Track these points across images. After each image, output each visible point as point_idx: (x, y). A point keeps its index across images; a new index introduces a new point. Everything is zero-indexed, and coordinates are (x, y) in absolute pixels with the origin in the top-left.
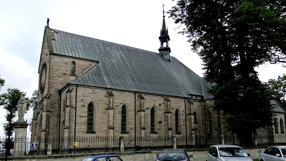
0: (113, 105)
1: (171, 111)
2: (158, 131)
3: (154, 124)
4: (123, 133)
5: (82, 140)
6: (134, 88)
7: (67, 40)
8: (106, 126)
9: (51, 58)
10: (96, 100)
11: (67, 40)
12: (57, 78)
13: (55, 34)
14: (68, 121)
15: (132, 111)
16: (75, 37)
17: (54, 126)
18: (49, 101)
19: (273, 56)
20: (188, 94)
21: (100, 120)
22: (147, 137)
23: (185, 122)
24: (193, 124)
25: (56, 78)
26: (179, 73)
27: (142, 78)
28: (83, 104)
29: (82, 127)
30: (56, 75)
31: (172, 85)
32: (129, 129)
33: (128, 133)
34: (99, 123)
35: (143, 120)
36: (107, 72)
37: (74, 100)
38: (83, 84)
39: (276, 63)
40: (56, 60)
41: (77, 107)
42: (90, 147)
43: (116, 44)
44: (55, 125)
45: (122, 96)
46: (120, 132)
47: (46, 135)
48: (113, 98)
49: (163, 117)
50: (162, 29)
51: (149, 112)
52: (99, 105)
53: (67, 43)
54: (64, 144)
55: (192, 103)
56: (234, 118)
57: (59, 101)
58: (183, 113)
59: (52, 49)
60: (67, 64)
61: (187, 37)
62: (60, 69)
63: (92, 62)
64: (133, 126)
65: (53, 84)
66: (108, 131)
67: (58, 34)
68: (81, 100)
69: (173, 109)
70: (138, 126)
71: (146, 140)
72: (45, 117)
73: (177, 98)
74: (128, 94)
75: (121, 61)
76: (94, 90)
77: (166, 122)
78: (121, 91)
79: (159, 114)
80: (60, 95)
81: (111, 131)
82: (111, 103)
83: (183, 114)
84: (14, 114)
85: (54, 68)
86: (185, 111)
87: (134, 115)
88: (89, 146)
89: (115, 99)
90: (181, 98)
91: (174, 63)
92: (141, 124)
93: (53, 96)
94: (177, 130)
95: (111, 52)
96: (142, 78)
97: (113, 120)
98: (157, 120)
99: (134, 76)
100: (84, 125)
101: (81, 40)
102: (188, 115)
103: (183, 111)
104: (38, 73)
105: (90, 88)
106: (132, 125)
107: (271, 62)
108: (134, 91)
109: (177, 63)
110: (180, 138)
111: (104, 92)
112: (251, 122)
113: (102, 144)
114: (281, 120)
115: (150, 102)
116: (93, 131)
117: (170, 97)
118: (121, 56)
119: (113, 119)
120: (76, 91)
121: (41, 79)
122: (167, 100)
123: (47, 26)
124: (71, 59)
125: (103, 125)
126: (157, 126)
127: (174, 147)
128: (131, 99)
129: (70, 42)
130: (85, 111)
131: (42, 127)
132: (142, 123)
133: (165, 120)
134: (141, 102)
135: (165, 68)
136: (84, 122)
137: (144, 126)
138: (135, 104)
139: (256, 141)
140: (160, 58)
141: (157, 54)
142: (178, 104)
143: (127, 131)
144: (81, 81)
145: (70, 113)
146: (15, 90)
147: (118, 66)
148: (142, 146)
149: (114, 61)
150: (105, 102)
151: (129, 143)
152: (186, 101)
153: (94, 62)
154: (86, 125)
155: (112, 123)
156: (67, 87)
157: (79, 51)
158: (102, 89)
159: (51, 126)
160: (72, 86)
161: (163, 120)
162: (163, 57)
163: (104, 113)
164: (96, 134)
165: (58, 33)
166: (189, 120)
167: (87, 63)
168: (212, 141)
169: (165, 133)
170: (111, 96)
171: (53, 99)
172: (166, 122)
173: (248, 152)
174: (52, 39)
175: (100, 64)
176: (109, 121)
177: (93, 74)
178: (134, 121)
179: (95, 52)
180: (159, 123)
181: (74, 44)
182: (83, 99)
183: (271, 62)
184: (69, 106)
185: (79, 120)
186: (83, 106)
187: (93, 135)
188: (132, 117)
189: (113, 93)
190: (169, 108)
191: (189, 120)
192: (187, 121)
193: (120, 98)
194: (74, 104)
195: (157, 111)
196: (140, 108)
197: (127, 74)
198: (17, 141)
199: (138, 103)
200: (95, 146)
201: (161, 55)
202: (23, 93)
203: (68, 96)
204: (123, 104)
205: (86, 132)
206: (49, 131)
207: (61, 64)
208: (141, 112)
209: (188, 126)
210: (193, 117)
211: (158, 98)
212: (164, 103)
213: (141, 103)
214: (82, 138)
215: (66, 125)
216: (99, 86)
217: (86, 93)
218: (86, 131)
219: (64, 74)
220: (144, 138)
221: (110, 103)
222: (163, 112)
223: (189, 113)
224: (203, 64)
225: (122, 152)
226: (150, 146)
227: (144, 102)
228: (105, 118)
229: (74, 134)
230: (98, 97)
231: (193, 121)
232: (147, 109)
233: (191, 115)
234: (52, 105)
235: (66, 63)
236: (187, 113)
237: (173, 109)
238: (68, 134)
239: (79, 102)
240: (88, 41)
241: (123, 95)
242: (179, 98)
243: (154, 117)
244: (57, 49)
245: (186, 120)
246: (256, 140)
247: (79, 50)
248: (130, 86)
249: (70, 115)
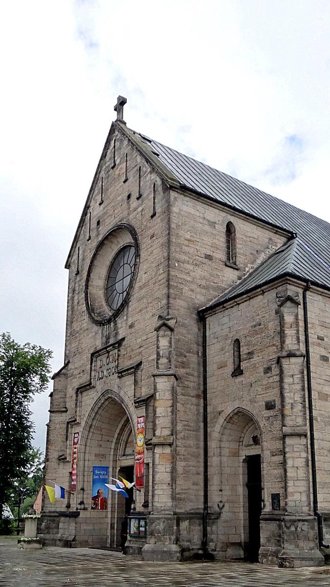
30: (187, 258)
40: (185, 208)
57: (198, 345)
85: (181, 233)
121: (90, 283)
171: (182, 335)
203: (289, 319)
215: (288, 421)
235: (212, 224)
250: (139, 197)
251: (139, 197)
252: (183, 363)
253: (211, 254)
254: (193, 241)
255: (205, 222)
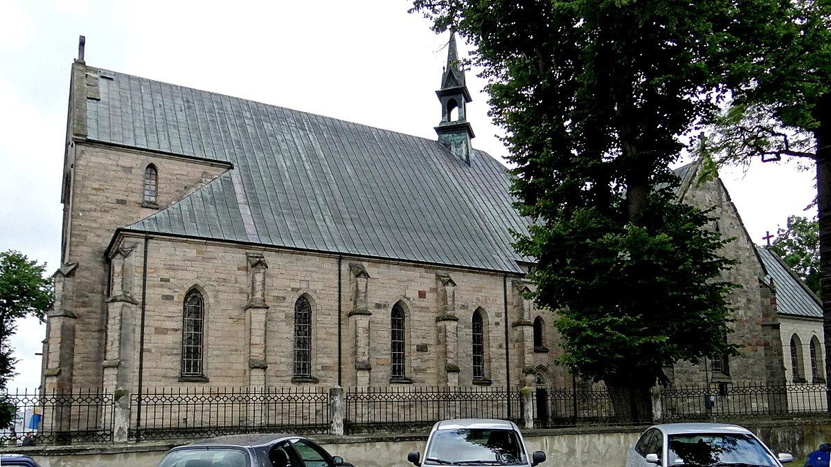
0: (263, 295)
1: (459, 313)
2: (414, 376)
3: (404, 354)
4: (300, 382)
5: (166, 400)
6: (338, 242)
7: (136, 100)
8: (242, 359)
9: (78, 153)
10: (210, 279)
11: (136, 100)
12: (99, 214)
13: (103, 82)
14: (117, 344)
15: (329, 315)
16: (166, 91)
17: (89, 359)
18: (71, 283)
19: (772, 139)
20: (517, 261)
21: (222, 343)
22: (600, 392)
23: (504, 346)
24: (530, 353)
25: (94, 214)
26: (496, 197)
27: (370, 213)
28: (167, 292)
29: (163, 365)
30: (93, 207)
31: (467, 235)
32: (319, 367)
33: (316, 381)
34: (219, 349)
35: (362, 341)
36: (255, 197)
37: (138, 281)
38: (168, 232)
39: (779, 158)
40: (94, 159)
41: (146, 300)
42: (190, 423)
43: (299, 112)
44: (92, 356)
45: (295, 268)
46: (290, 378)
47: (60, 386)
48: (264, 273)
49: (433, 333)
50: (446, 67)
51: (385, 317)
52: (221, 296)
53: (138, 108)
54: (103, 414)
55: (526, 288)
56: (584, 329)
57: (103, 284)
58: (498, 320)
59: (84, 127)
60: (131, 172)
61: (478, 76)
62: (108, 187)
63: (212, 165)
64: (332, 361)
65: (83, 233)
66: (247, 373)
67: (113, 84)
68: (162, 280)
69: (463, 307)
70: (347, 359)
71: (370, 401)
72: (58, 334)
73: (478, 273)
74: (316, 260)
75: (306, 164)
76: (204, 248)
77: (441, 348)
78: (293, 253)
79: (420, 326)
80: (107, 265)
81: (258, 374)
82: (259, 287)
83: (497, 324)
84: (10, 326)
85: (87, 183)
86: (504, 315)
87: (337, 326)
88: (185, 420)
89: (272, 276)
90: (491, 275)
91: (482, 169)
92: (355, 353)
93: (87, 269)
94: (477, 372)
95: (279, 138)
96: (370, 213)
97: (265, 341)
98: (413, 338)
99: (343, 209)
100: (169, 355)
101: (185, 99)
102: (515, 325)
103: (498, 315)
104: (62, 202)
105: (190, 243)
106: (328, 357)
107: (763, 158)
108: (337, 253)
109: (493, 169)
110: (395, 395)
111: (239, 256)
112: (641, 342)
113: (229, 414)
114: (814, 342)
115: (385, 286)
116: (202, 376)
117: (454, 271)
118: (311, 150)
119: (263, 338)
120: (146, 252)
122: (445, 279)
123: (77, 58)
124: (143, 157)
125: (234, 358)
126: (412, 360)
127: (334, 426)
128: (326, 276)
129: (148, 106)
130: (175, 315)
131: (48, 364)
132: (360, 350)
133: (439, 342)
134: (357, 286)
135: (450, 184)
136: (171, 346)
137: (365, 358)
138: (340, 291)
139: (655, 407)
140: (438, 155)
141: (429, 142)
142: (471, 292)
143: (313, 374)
144: (164, 222)
145: (121, 318)
146: (11, 254)
147: (294, 178)
148: (359, 420)
149: (283, 163)
150: (242, 286)
151: (319, 411)
152: (509, 284)
153: (221, 167)
154: (179, 358)
155: (262, 350)
156: (119, 238)
157: (173, 134)
158: (231, 246)
159: (77, 359)
160: (131, 236)
161: (431, 340)
162: (448, 153)
163: (238, 320)
164: (210, 384)
165: (111, 79)
166: (517, 341)
167: (196, 170)
168: (590, 407)
169: (439, 382)
170: (259, 266)
171: (85, 277)
172: (441, 348)
173: (625, 443)
174: (88, 98)
175: (235, 172)
176: (250, 344)
177: (207, 200)
178: (337, 346)
179: (226, 136)
180: (418, 350)
181: (158, 111)
182: (166, 276)
183: (763, 158)
184: (119, 299)
185: (152, 341)
186: (168, 298)
187: (199, 387)
188: (330, 330)
189: (266, 258)
190: (450, 303)
191: (517, 341)
192: (510, 345)
193: (287, 277)
194: (137, 292)
195: (412, 313)
196: (355, 303)
197: (321, 202)
198: (65, 401)
199: (347, 290)
200: (214, 420)
201: (444, 146)
202: (36, 265)
204: (301, 292)
205: (177, 377)
206: (72, 375)
207: (112, 173)
208: (358, 317)
209: (514, 359)
210: (529, 331)
211: (417, 273)
212: (434, 290)
213: (357, 291)
214: (172, 394)
215: (109, 356)
216: (220, 236)
217: (177, 258)
218: (177, 374)
219: (122, 202)
220: (286, 396)
221: (253, 288)
222: (431, 316)
223: (516, 320)
224: (508, 158)
225: (118, 443)
226: (390, 419)
227: (367, 287)
228: (241, 334)
229: (137, 383)
230: (220, 272)
231: (530, 343)
232: (378, 306)
233: (523, 325)
234: (83, 296)
235: (128, 170)
236: (510, 321)
237: (463, 307)
238: (115, 383)
239: (154, 286)
240: (207, 103)
241: (299, 263)
242: (484, 274)
243: (403, 332)
244: (101, 126)
245: (509, 342)
246: (659, 403)
247: (173, 131)
248: (325, 237)
249: (121, 327)
250: (101, 116)
251: (101, 116)
252: (84, 302)
253: (125, 198)
254: (102, 190)
255: (119, 169)
